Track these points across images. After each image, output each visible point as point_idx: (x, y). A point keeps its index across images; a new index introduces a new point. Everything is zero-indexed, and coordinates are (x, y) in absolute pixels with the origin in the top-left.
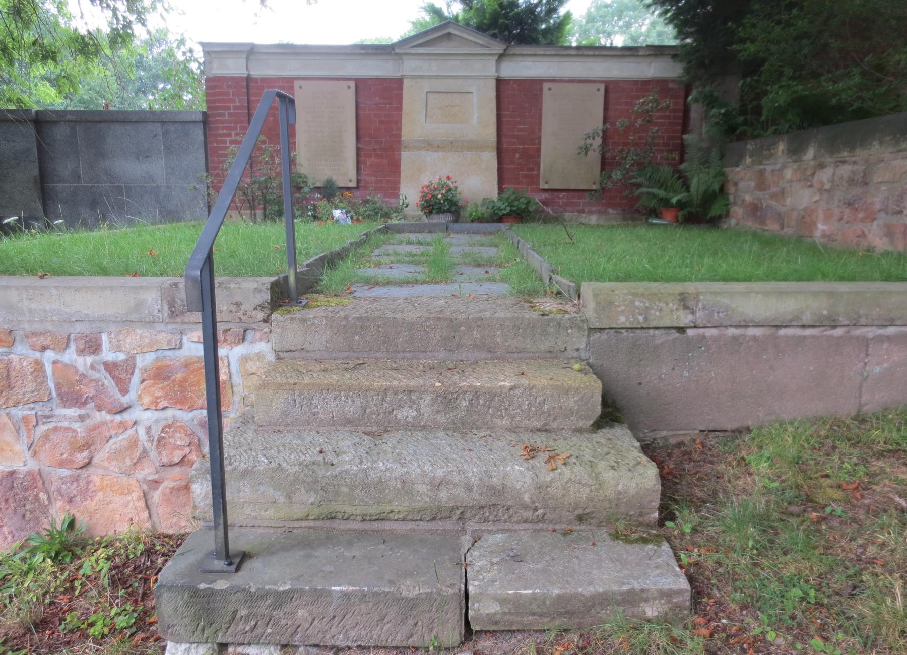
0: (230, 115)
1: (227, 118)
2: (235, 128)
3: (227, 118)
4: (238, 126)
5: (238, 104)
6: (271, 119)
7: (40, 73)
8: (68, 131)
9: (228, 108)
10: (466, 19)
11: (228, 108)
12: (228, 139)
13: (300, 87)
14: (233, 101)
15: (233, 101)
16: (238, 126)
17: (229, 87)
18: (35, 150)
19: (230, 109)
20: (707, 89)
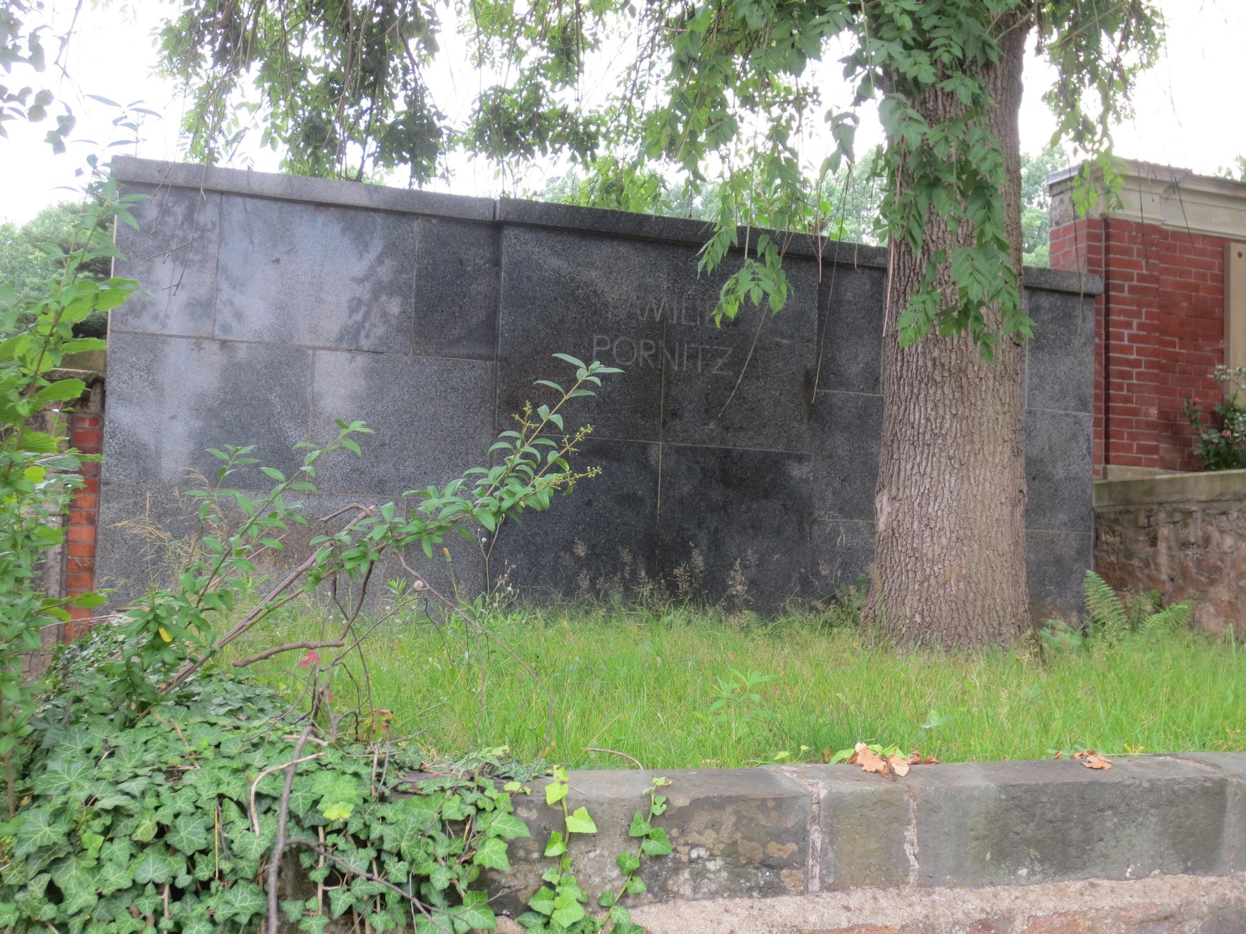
0: (1132, 289)
1: (1126, 294)
2: (1137, 315)
3: (1126, 294)
4: (1144, 310)
5: (1144, 272)
6: (1185, 304)
7: (618, 877)
8: (867, 287)
9: (1129, 277)
10: (443, 587)
11: (1129, 277)
12: (1126, 332)
13: (1240, 255)
14: (1137, 265)
15: (1137, 265)
16: (1144, 310)
17: (1133, 240)
18: (814, 315)
19: (1138, 275)
20: (397, 520)
